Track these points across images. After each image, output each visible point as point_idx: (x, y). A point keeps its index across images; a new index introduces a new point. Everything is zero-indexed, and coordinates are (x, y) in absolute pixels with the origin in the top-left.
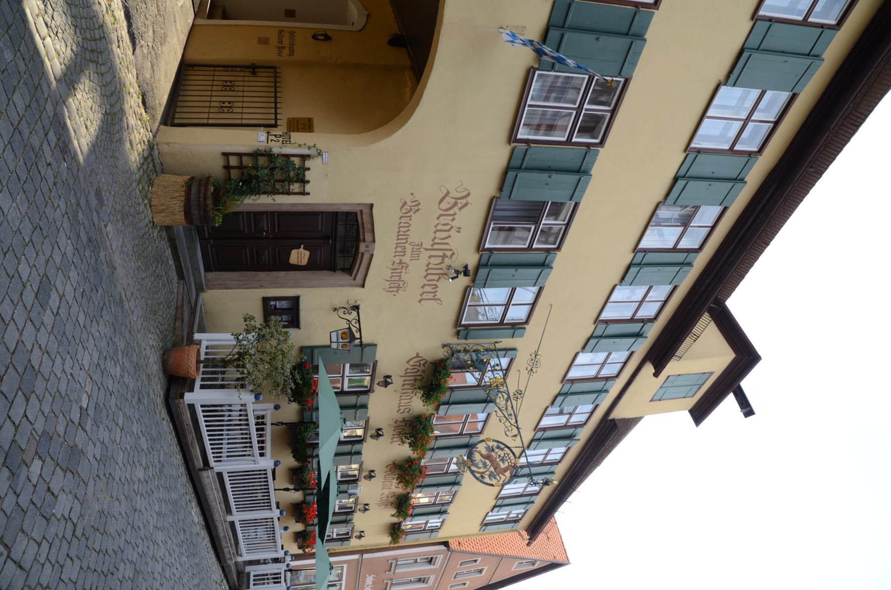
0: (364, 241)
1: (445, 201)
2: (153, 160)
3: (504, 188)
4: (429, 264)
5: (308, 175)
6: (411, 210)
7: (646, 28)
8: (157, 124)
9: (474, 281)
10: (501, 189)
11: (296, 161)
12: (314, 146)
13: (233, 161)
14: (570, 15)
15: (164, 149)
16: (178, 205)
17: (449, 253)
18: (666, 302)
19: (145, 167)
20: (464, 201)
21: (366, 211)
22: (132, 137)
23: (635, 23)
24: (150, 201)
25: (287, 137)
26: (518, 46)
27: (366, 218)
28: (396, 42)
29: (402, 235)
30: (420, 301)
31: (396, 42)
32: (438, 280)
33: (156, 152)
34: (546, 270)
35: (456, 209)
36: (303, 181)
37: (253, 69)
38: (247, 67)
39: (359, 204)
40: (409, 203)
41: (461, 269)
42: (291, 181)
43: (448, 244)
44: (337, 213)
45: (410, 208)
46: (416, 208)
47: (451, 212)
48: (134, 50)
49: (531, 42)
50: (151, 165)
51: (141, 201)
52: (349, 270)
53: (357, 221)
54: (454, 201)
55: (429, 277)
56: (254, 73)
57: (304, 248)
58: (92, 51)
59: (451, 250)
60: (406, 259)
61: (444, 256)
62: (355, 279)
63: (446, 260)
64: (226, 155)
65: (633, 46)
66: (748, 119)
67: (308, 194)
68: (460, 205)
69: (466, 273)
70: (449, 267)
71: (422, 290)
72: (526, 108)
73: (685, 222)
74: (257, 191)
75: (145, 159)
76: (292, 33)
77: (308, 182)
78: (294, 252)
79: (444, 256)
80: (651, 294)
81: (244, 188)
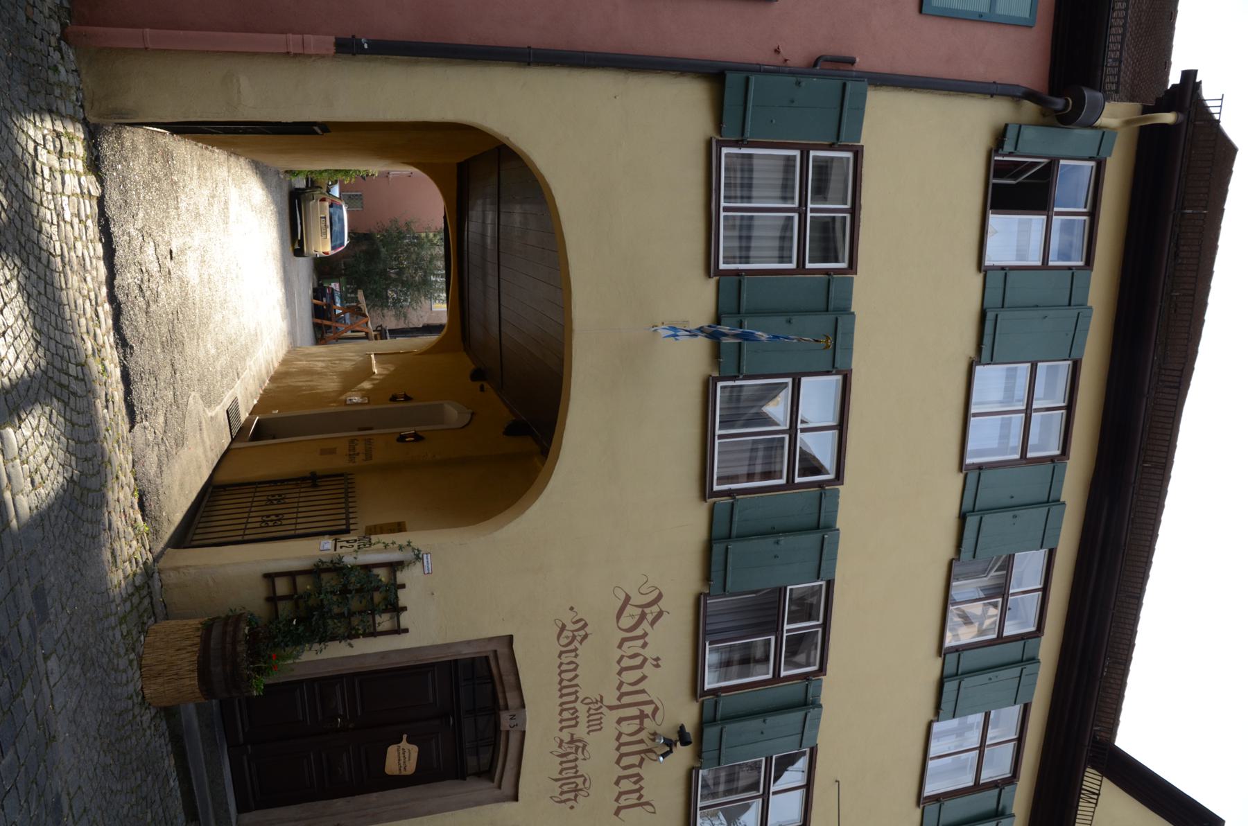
0: (507, 708)
1: (626, 613)
2: (150, 594)
3: (713, 575)
4: (620, 734)
5: (404, 597)
6: (574, 637)
7: (849, 300)
8: (162, 545)
9: (699, 755)
10: (707, 577)
11: (383, 574)
12: (409, 544)
13: (282, 587)
14: (744, 296)
15: (171, 578)
16: (187, 661)
17: (648, 709)
18: (1020, 741)
19: (135, 600)
20: (655, 609)
21: (502, 651)
22: (117, 546)
23: (832, 294)
24: (140, 658)
25: (366, 541)
26: (684, 340)
27: (504, 665)
28: (514, 430)
29: (567, 687)
30: (617, 813)
31: (514, 430)
32: (640, 765)
33: (157, 585)
34: (812, 713)
35: (645, 625)
36: (395, 609)
37: (313, 480)
38: (303, 479)
39: (491, 639)
40: (570, 626)
41: (674, 737)
42: (373, 611)
43: (643, 691)
44: (456, 661)
45: (573, 634)
46: (582, 633)
48: (132, 427)
49: (701, 329)
50: (146, 601)
51: (122, 652)
52: (487, 773)
53: (490, 670)
54: (639, 611)
55: (626, 761)
56: (315, 485)
57: (409, 741)
58: (61, 385)
59: (651, 702)
60: (581, 732)
61: (642, 716)
62: (499, 787)
63: (647, 722)
64: (270, 577)
65: (840, 323)
66: (1028, 410)
67: (406, 631)
68: (650, 618)
69: (683, 738)
70: (654, 735)
71: (617, 790)
72: (717, 441)
73: (1000, 591)
74: (326, 637)
75: (137, 589)
76: (368, 441)
77: (404, 609)
78: (392, 750)
79: (642, 716)
80: (991, 733)
81: (301, 628)
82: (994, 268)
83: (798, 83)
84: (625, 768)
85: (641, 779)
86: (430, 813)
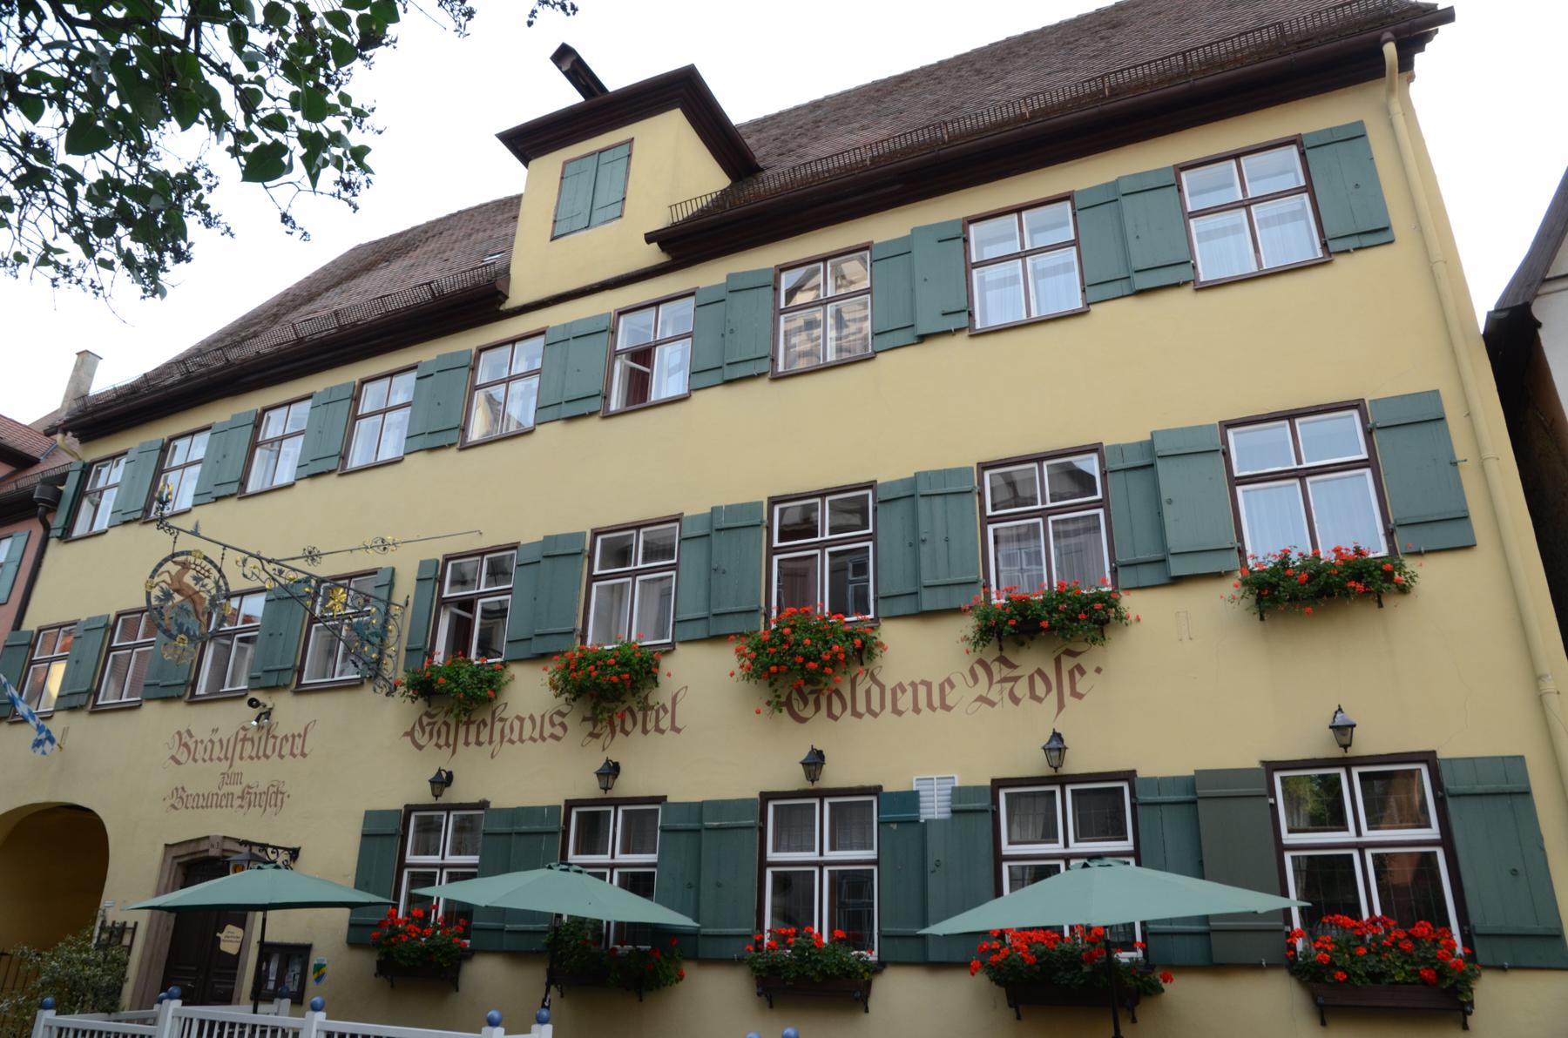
17: (241, 734)
21: (175, 852)
27: (182, 851)
30: (678, 731)
34: (1160, 448)
47: (192, 747)
55: (269, 752)
60: (237, 789)
78: (224, 947)
82: (1084, 298)
83: (1170, 502)
84: (883, 707)
85: (900, 685)
86: (1045, 928)
